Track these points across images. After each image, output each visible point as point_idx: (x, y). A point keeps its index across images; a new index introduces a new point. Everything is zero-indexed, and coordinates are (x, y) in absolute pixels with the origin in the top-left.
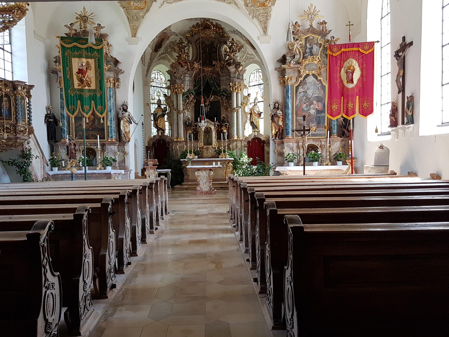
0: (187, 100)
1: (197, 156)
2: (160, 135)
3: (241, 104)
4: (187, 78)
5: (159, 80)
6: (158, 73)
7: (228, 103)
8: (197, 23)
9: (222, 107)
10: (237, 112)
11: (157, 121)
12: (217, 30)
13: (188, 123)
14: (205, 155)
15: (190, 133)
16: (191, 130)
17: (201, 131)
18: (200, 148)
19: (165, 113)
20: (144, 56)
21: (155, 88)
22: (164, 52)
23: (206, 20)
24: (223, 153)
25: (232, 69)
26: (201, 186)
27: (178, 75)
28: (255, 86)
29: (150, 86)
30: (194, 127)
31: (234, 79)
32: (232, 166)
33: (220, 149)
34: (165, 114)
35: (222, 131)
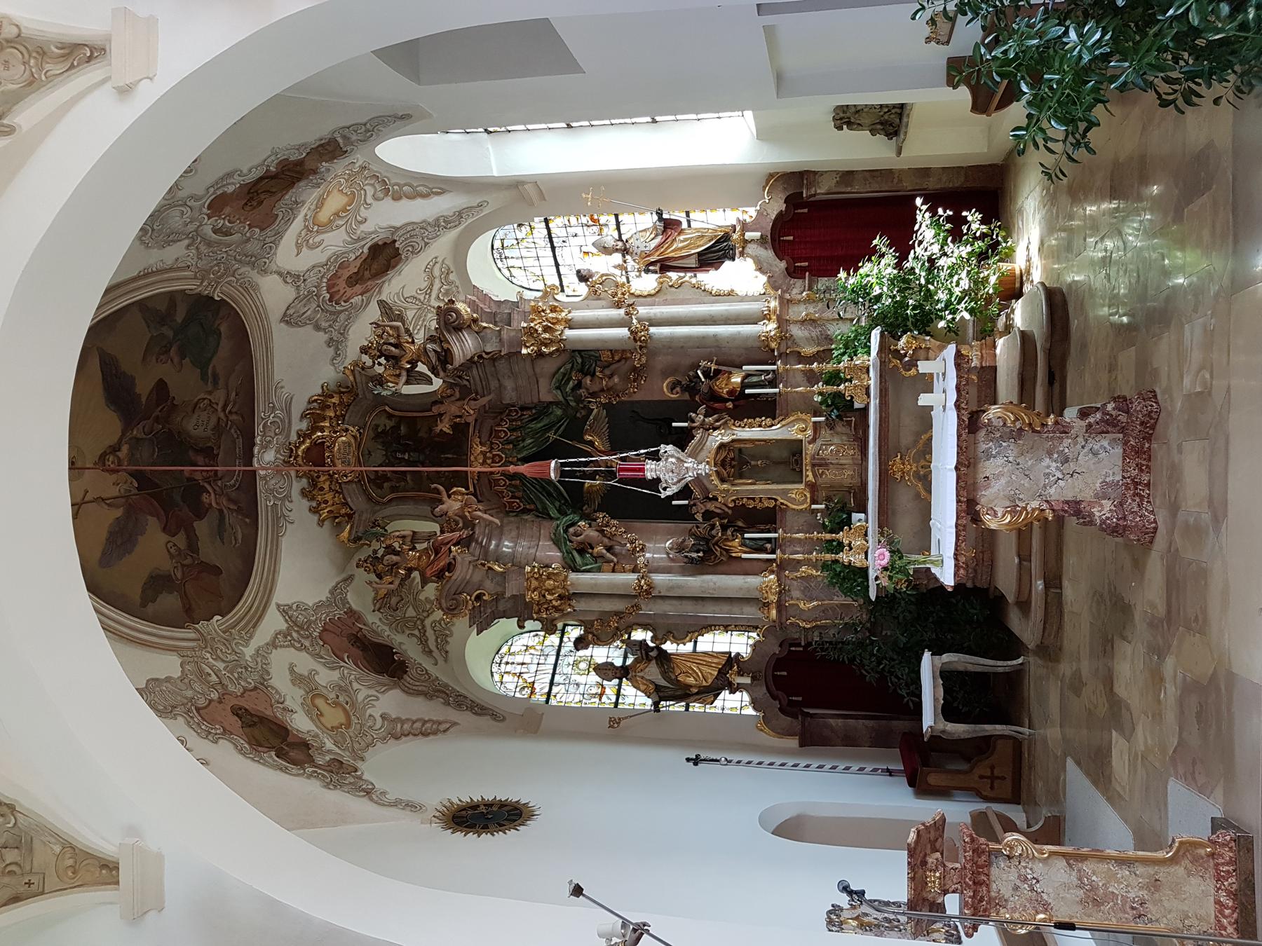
0: (596, 550)
1: (856, 516)
2: (747, 680)
3: (618, 305)
4: (507, 547)
5: (527, 659)
6: (504, 660)
8: (304, 493)
9: (630, 395)
10: (651, 325)
12: (332, 414)
13: (698, 552)
14: (847, 476)
15: (742, 545)
16: (727, 540)
18: (814, 502)
19: (652, 649)
20: (414, 722)
21: (557, 678)
22: (416, 632)
23: (290, 457)
24: (842, 387)
25: (464, 346)
26: (1087, 495)
27: (489, 585)
28: (557, 265)
29: (547, 701)
30: (713, 527)
31: (505, 335)
32: (914, 338)
33: (821, 403)
34: (658, 648)
35: (738, 396)
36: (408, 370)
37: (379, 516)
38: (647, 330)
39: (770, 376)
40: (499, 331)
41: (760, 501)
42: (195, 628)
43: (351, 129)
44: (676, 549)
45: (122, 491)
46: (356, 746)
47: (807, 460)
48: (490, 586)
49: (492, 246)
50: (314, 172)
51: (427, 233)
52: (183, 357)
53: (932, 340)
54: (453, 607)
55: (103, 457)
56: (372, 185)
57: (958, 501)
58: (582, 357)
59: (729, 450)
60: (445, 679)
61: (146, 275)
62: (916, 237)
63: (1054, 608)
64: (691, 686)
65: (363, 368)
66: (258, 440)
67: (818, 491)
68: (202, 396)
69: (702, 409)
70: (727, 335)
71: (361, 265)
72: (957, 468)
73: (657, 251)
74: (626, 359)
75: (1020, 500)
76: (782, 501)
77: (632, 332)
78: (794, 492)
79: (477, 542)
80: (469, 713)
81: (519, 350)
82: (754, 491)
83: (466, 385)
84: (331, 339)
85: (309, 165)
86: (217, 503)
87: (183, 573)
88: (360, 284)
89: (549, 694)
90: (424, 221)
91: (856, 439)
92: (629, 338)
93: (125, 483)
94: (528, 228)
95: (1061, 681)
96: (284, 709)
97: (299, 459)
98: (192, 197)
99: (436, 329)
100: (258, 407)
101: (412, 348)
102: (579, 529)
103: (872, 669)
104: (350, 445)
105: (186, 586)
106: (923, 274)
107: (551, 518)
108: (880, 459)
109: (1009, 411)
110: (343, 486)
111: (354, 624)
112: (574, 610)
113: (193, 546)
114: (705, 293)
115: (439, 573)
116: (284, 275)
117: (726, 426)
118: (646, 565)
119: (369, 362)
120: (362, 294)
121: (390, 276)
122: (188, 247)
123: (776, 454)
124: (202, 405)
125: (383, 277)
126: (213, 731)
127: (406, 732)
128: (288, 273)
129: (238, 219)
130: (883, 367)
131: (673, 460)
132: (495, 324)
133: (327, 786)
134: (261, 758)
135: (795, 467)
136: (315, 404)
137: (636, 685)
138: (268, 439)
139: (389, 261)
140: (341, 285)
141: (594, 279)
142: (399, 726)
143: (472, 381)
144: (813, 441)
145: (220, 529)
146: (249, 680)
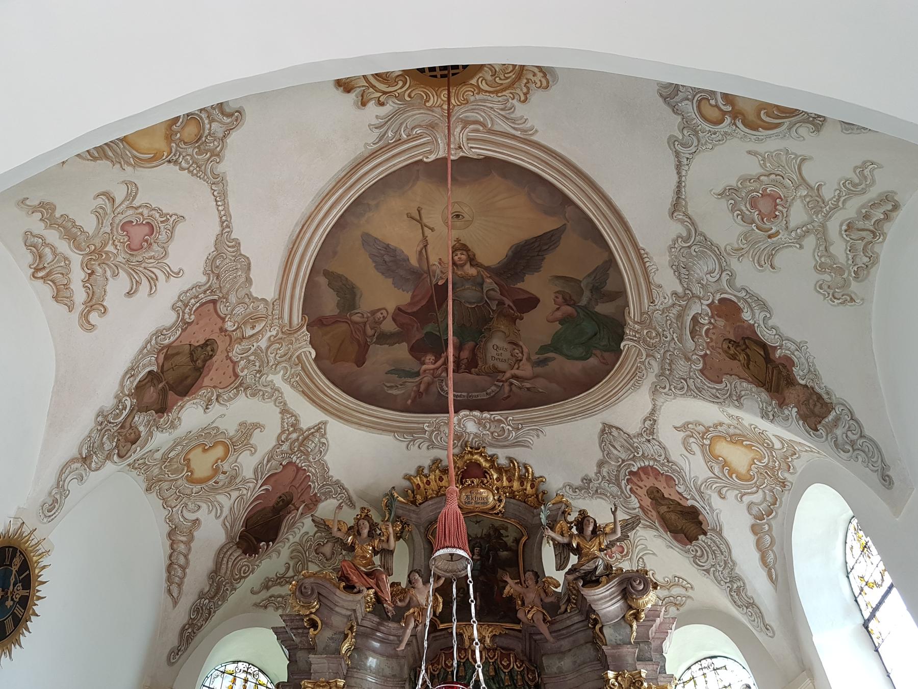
8: (436, 462)
20: (186, 556)
22: (291, 573)
23: (471, 448)
36: (569, 545)
37: (416, 533)
40: (630, 643)
42: (302, 326)
43: (851, 422)
45: (434, 267)
46: (165, 485)
48: (323, 636)
49: (715, 657)
50: (782, 404)
52: (562, 321)
54: (303, 590)
55: (464, 248)
56: (765, 499)
60: (233, 598)
61: (641, 257)
65: (564, 512)
66: (486, 415)
68: (525, 350)
79: (379, 624)
80: (185, 621)
83: (560, 608)
85: (791, 394)
86: (425, 371)
87: (357, 323)
88: (651, 503)
90: (734, 564)
93: (441, 272)
96: (210, 400)
98: (732, 275)
99: (621, 569)
104: (486, 503)
105: (345, 324)
111: (304, 502)
113: (384, 338)
115: (345, 577)
116: (652, 418)
120: (641, 507)
121: (665, 536)
122: (675, 293)
124: (517, 351)
125: (662, 527)
126: (187, 310)
127: (175, 546)
128: (655, 421)
129: (711, 339)
132: (637, 643)
133: (100, 413)
134: (149, 353)
138: (488, 426)
139: (682, 531)
140: (649, 482)
142: (184, 539)
143: (565, 616)
145: (399, 371)
146: (246, 372)
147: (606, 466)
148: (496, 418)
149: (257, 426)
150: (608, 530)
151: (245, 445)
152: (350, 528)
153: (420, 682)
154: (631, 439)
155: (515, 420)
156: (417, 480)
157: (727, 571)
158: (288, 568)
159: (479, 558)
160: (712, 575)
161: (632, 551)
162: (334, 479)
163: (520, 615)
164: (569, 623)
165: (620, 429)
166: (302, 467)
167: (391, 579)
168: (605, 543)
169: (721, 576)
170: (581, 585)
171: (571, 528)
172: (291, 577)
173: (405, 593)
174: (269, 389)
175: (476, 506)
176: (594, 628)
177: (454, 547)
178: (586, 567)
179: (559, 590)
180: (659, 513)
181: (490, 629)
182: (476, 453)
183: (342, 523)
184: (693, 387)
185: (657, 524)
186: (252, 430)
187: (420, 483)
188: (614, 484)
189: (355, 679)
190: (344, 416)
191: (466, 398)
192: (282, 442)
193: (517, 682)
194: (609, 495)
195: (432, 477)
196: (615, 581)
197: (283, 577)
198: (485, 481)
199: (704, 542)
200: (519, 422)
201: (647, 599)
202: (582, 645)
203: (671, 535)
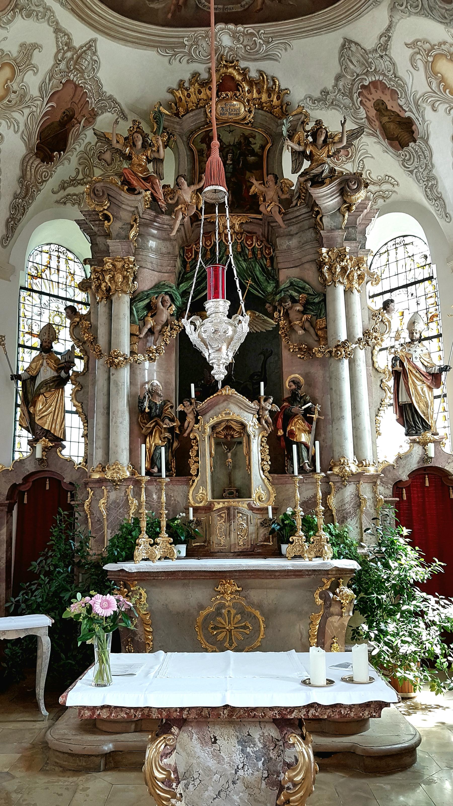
0: (150, 319)
1: (183, 548)
2: (39, 454)
3: (366, 333)
6: (61, 255)
7: (311, 330)
8: (195, 75)
11: (34, 405)
16: (161, 433)
17: (201, 437)
18: (196, 510)
21: (45, 298)
22: (80, 176)
23: (226, 61)
24: (302, 533)
30: (172, 420)
31: (338, 233)
32: (351, 602)
33: (285, 514)
34: (68, 378)
36: (304, 152)
37: (179, 141)
38: (346, 357)
39: (308, 468)
41: (196, 462)
44: (152, 389)
47: (233, 502)
51: (421, 170)
53: (349, 618)
54: (96, 193)
57: (182, 709)
58: (319, 303)
59: (241, 433)
60: (39, 197)
62: (442, 599)
63: (84, 764)
64: (34, 407)
65: (303, 122)
66: (240, 28)
67: (205, 513)
69: (276, 408)
70: (344, 428)
71: (393, 112)
72: (227, 706)
73: (413, 367)
74: (319, 341)
75: (187, 786)
76: (196, 481)
77: (344, 343)
78: (204, 492)
79: (156, 217)
80: (8, 216)
81: (325, 246)
82: (204, 456)
83: (292, 203)
84: (328, 93)
88: (376, 114)
89: (32, 290)
90: (433, 166)
91: (254, 546)
92: (339, 341)
94: (424, 264)
95: (7, 773)
97: (223, 70)
100: (269, 27)
101: (324, 155)
102: (169, 305)
103: (43, 567)
104: (238, 114)
106: (412, 608)
107: (178, 285)
108: (236, 571)
109: (306, 773)
110: (203, 109)
112: (98, 303)
114: (377, 410)
117: (261, 429)
118: (136, 361)
119: (308, 128)
120: (367, 117)
121: (383, 142)
123: (238, 476)
130: (323, 572)
131: (230, 333)
132: (347, 228)
135: (226, 492)
136: (272, 83)
137: (36, 360)
138: (242, 40)
139: (397, 139)
140: (376, 95)
141: (386, 315)
143: (296, 209)
144: (251, 508)
147: (342, 79)
148: (249, 31)
149: (35, 46)
150: (336, 139)
151: (28, 66)
152: (126, 139)
153: (199, 264)
154: (367, 54)
155: (266, 34)
156: (179, 94)
157: (426, 172)
158: (78, 173)
159: (231, 162)
160: (414, 175)
161: (355, 155)
162: (108, 94)
163: (262, 208)
164: (298, 214)
165: (359, 45)
166: (79, 84)
167: (163, 183)
168: (333, 151)
169: (421, 176)
170: (309, 185)
171: (307, 136)
172: (81, 180)
173: (174, 193)
174: (41, 9)
175: (230, 117)
176: (316, 217)
177: (217, 185)
178: (315, 171)
179: (293, 188)
180: (381, 122)
181: (239, 219)
182: (231, 66)
183: (119, 136)
184: (426, 6)
185: (378, 133)
186: (32, 51)
187: (181, 96)
188: (347, 96)
189: (141, 256)
190: (112, 33)
191: (221, 11)
192: (59, 61)
193: (257, 256)
194: (342, 106)
195: (192, 90)
196: (336, 182)
197: (75, 180)
198: (238, 94)
199: (413, 148)
200: (269, 36)
201: (358, 196)
202: (306, 230)
203: (389, 143)
